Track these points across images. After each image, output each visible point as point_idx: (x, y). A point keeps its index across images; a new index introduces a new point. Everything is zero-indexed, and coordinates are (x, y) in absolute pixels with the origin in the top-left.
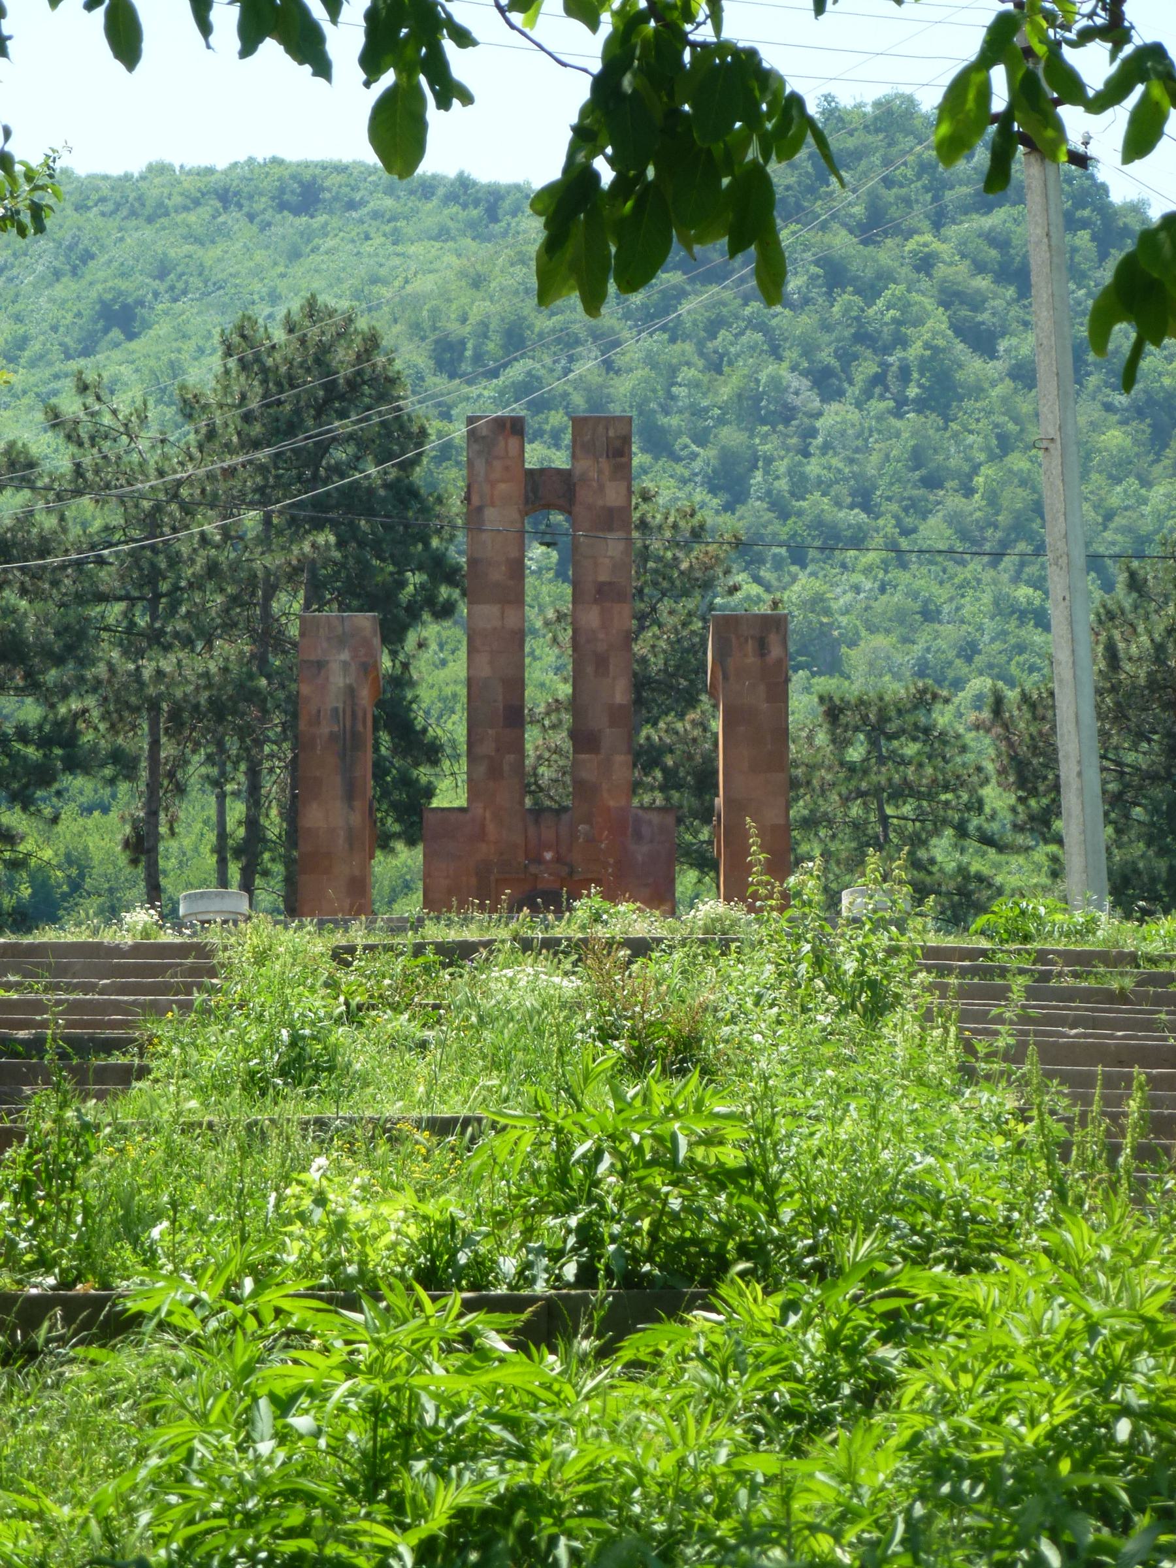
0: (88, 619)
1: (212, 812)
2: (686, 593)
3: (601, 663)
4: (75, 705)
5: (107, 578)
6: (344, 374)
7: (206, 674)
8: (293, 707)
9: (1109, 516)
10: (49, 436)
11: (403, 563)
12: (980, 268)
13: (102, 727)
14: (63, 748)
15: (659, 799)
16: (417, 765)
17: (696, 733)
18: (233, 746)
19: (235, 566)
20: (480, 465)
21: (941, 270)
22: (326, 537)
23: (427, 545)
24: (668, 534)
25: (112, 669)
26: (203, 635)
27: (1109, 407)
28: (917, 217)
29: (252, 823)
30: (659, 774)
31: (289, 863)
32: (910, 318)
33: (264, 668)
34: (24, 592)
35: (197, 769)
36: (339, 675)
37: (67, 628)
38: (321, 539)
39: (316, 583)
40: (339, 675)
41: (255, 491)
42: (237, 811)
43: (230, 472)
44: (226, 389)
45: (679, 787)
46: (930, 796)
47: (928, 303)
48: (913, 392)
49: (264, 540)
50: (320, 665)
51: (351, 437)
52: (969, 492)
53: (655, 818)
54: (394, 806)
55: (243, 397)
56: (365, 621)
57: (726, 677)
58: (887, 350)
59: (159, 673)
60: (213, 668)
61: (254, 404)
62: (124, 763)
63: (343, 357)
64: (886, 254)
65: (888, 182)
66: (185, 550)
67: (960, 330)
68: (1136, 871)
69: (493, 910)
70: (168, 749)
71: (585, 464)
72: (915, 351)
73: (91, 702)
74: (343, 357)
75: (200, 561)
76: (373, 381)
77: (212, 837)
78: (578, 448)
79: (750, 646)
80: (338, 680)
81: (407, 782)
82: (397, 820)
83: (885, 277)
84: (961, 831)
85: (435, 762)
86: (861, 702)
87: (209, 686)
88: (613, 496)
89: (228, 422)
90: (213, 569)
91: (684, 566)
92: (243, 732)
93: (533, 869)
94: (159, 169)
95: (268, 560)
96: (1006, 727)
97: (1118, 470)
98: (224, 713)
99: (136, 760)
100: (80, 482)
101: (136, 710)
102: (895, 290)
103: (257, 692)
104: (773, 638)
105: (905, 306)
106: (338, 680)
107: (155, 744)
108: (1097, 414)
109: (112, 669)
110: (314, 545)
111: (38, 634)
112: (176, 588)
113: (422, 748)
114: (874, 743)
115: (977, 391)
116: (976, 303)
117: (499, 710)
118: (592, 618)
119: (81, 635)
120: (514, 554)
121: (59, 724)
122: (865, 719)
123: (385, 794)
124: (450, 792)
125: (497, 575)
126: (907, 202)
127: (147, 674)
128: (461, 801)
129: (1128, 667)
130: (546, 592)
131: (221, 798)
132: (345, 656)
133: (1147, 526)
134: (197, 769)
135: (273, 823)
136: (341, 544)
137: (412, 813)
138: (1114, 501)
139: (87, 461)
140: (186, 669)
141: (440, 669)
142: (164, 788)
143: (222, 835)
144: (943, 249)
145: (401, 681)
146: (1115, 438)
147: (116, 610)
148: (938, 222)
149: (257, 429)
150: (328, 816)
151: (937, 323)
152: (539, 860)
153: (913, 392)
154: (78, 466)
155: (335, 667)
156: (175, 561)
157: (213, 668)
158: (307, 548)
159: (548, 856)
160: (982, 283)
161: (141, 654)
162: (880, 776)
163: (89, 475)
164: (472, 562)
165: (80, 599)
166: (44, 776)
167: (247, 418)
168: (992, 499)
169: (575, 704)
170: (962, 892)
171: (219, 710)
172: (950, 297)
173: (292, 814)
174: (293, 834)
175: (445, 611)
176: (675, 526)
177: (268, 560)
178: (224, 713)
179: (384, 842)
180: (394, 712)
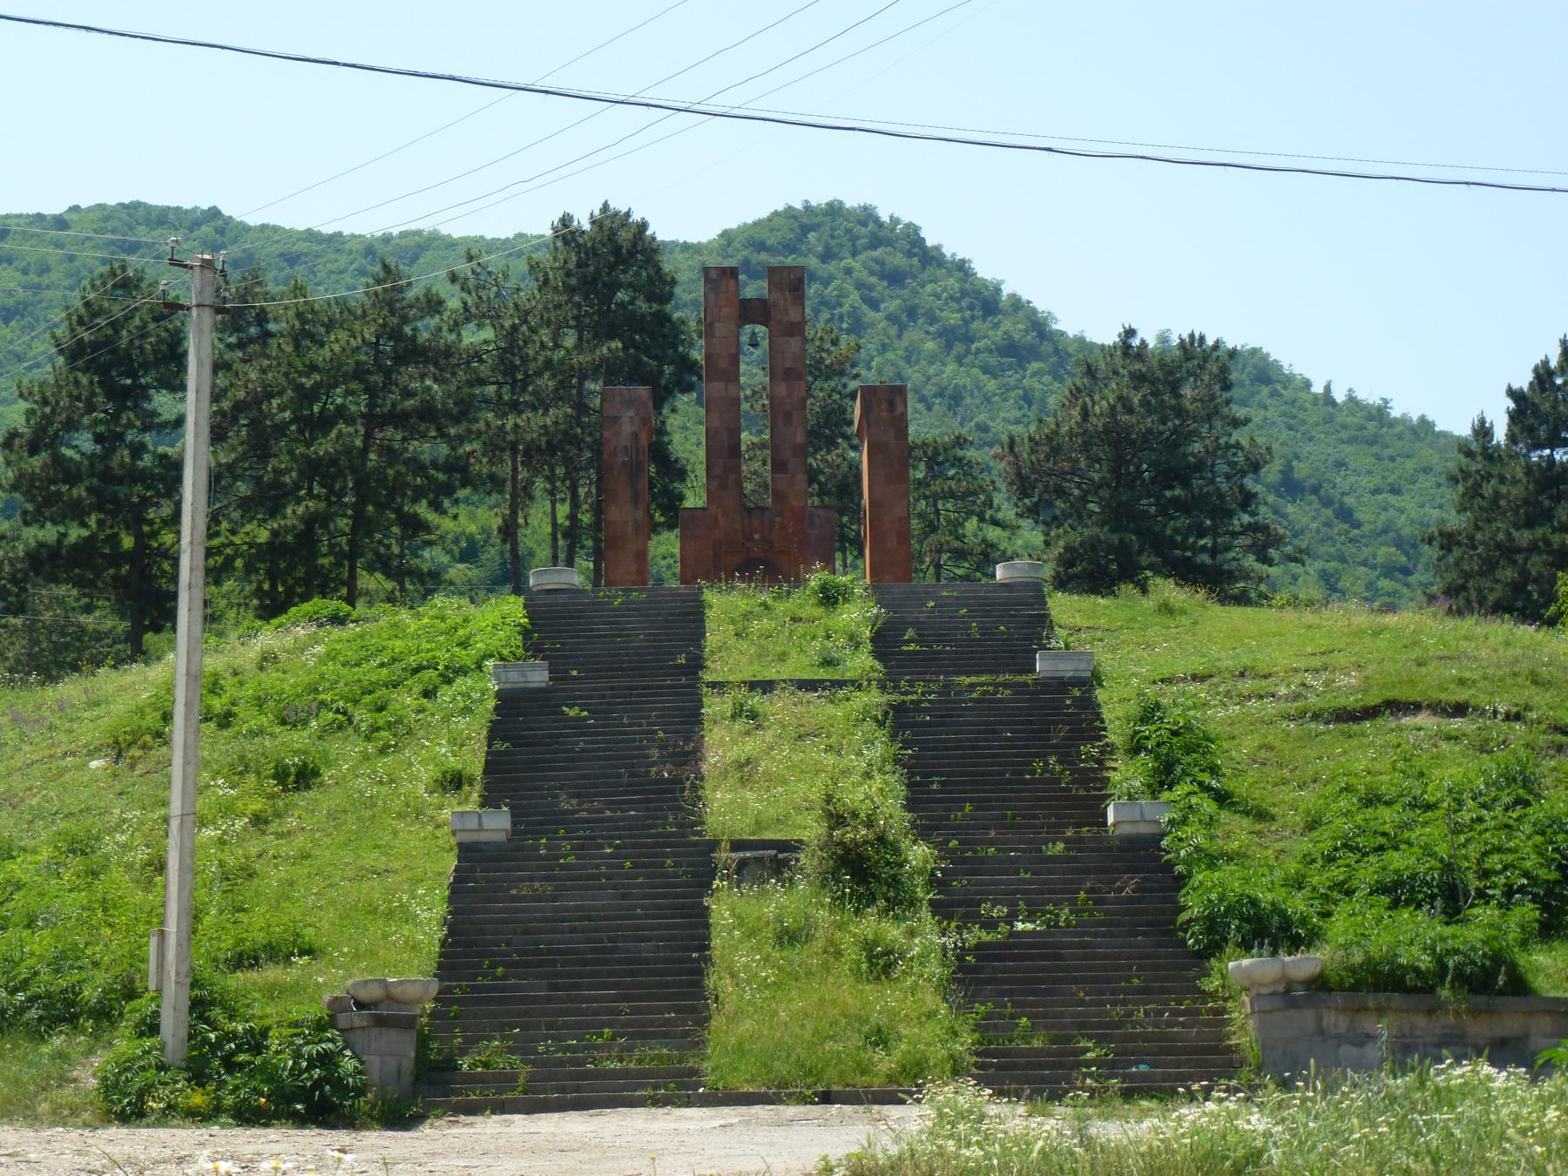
0: (474, 395)
1: (548, 509)
2: (828, 378)
3: (788, 417)
4: (468, 448)
5: (484, 371)
6: (626, 246)
7: (545, 426)
8: (598, 448)
9: (929, 379)
10: (450, 287)
11: (661, 361)
12: (872, 273)
13: (485, 460)
14: (459, 470)
15: (817, 501)
16: (672, 482)
17: (839, 460)
18: (560, 471)
19: (561, 362)
20: (712, 296)
21: (856, 274)
22: (617, 344)
23: (676, 350)
24: (818, 343)
25: (488, 424)
26: (541, 404)
27: (927, 333)
28: (846, 253)
29: (572, 517)
30: (816, 486)
31: (597, 541)
32: (843, 294)
33: (579, 422)
34: (436, 380)
35: (540, 484)
36: (628, 426)
37: (462, 400)
38: (613, 345)
39: (611, 371)
40: (628, 426)
41: (574, 318)
42: (563, 510)
43: (558, 307)
44: (555, 259)
45: (828, 494)
46: (963, 498)
47: (851, 288)
48: (845, 326)
49: (578, 346)
50: (616, 419)
51: (630, 285)
52: (869, 369)
53: (822, 513)
54: (659, 506)
55: (566, 262)
56: (643, 391)
57: (869, 425)
58: (833, 308)
59: (516, 426)
60: (548, 421)
61: (571, 266)
62: (496, 483)
63: (624, 236)
64: (832, 267)
65: (832, 237)
66: (531, 353)
67: (865, 300)
68: (1099, 541)
69: (750, 581)
70: (523, 474)
71: (776, 295)
72: (846, 308)
73: (476, 446)
74: (624, 236)
75: (541, 359)
76: (643, 252)
77: (549, 519)
78: (773, 285)
79: (884, 406)
80: (627, 429)
81: (666, 491)
82: (662, 515)
83: (832, 278)
84: (982, 519)
85: (683, 480)
86: (924, 444)
87: (546, 434)
88: (793, 315)
89: (557, 280)
90: (548, 363)
91: (828, 362)
92: (567, 461)
93: (748, 545)
94: (520, 236)
95: (581, 358)
96: (1016, 457)
97: (932, 359)
98: (549, 452)
99: (504, 481)
100: (467, 315)
101: (503, 450)
102: (837, 283)
103: (575, 436)
104: (898, 400)
105: (840, 289)
106: (627, 429)
107: (515, 469)
108: (922, 335)
109: (488, 424)
110: (609, 349)
111: (444, 404)
112: (528, 376)
113: (674, 470)
114: (930, 468)
115: (873, 325)
116: (871, 288)
117: (724, 451)
118: (782, 389)
119: (470, 404)
120: (733, 351)
121: (457, 458)
122: (925, 453)
123: (654, 499)
124: (694, 498)
125: (723, 364)
126: (841, 245)
127: (509, 427)
128: (700, 504)
129: (1094, 420)
130: (752, 373)
131: (553, 504)
132: (631, 413)
133: (945, 383)
134: (540, 484)
135: (586, 518)
136: (625, 349)
137: (671, 505)
138: (931, 371)
139: (470, 301)
140: (534, 423)
141: (687, 429)
142: (521, 497)
143: (554, 524)
144: (856, 265)
145: (661, 431)
146: (930, 345)
147: (491, 389)
148: (854, 254)
149: (573, 281)
150: (621, 513)
151: (854, 297)
152: (751, 539)
153: (845, 326)
154: (465, 304)
155: (625, 420)
156: (525, 359)
157: (548, 421)
158: (605, 350)
159: (757, 537)
160: (873, 280)
161: (505, 415)
162: (936, 486)
163: (473, 310)
164: (708, 357)
165: (470, 384)
166: (448, 490)
167: (568, 274)
168: (880, 372)
169: (774, 446)
170: (985, 554)
171: (551, 449)
172: (860, 285)
173: (598, 510)
174: (597, 526)
175: (688, 388)
176: (821, 339)
177: (581, 358)
178: (549, 452)
179: (655, 528)
180: (660, 453)
